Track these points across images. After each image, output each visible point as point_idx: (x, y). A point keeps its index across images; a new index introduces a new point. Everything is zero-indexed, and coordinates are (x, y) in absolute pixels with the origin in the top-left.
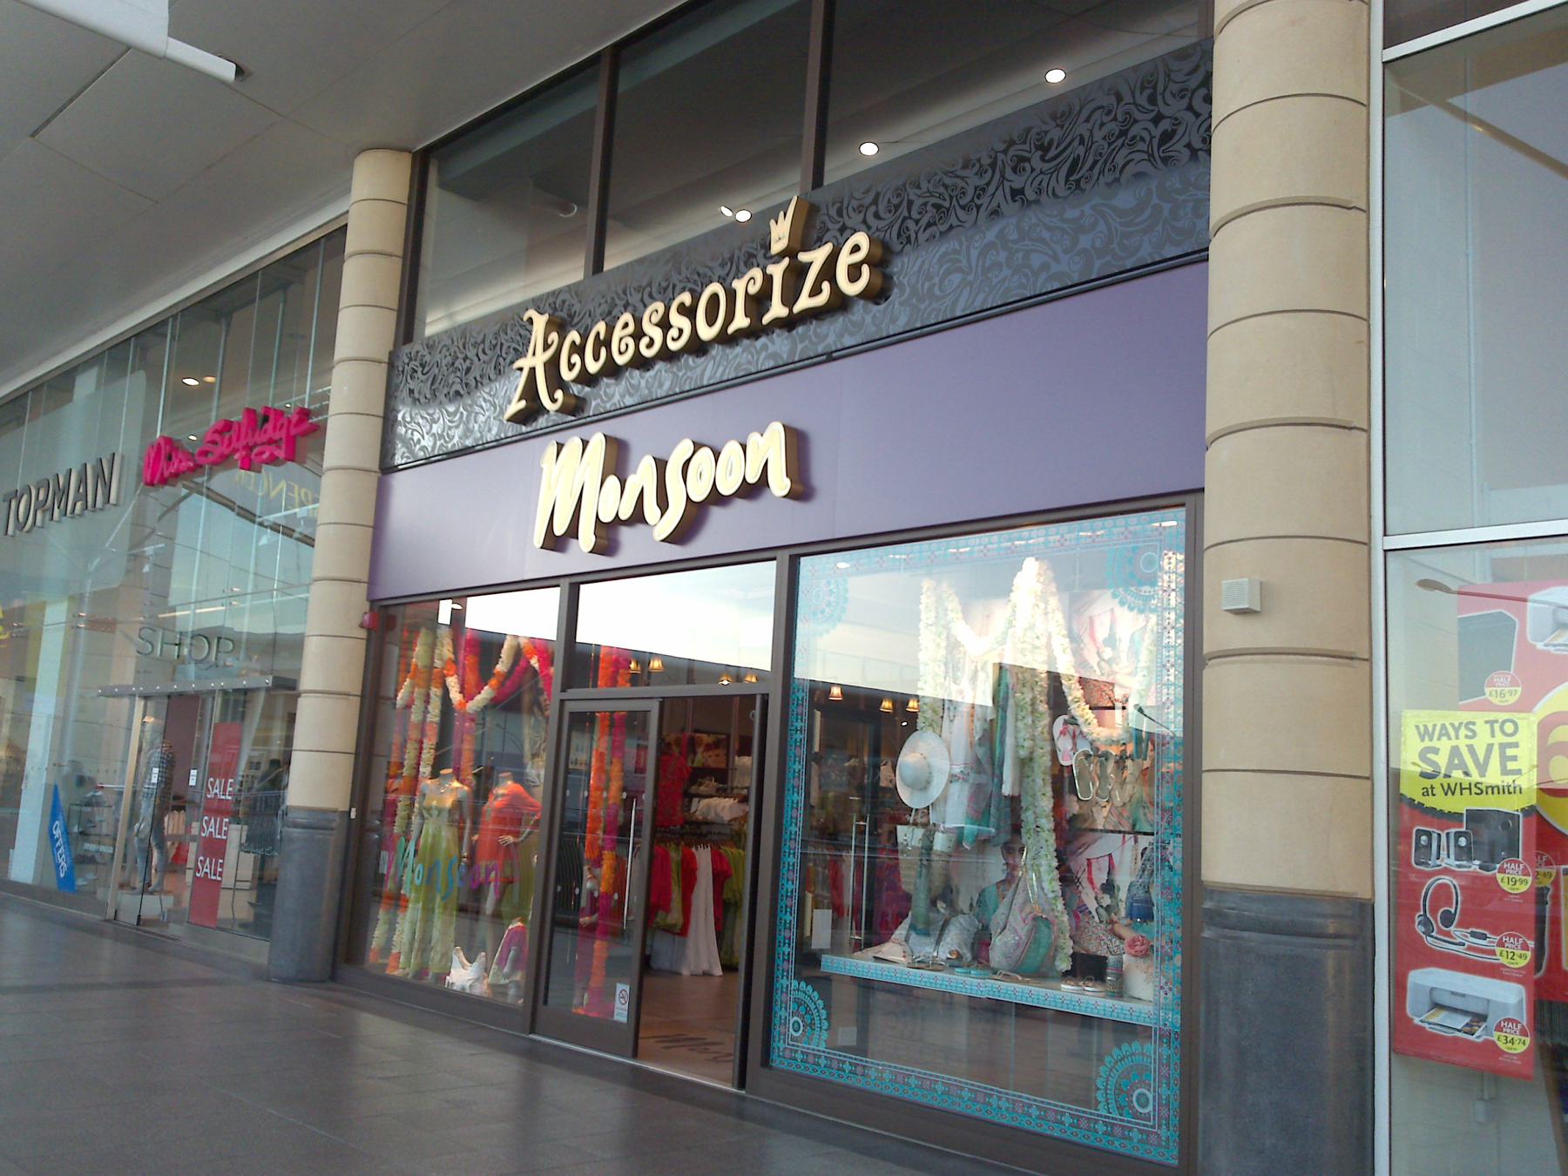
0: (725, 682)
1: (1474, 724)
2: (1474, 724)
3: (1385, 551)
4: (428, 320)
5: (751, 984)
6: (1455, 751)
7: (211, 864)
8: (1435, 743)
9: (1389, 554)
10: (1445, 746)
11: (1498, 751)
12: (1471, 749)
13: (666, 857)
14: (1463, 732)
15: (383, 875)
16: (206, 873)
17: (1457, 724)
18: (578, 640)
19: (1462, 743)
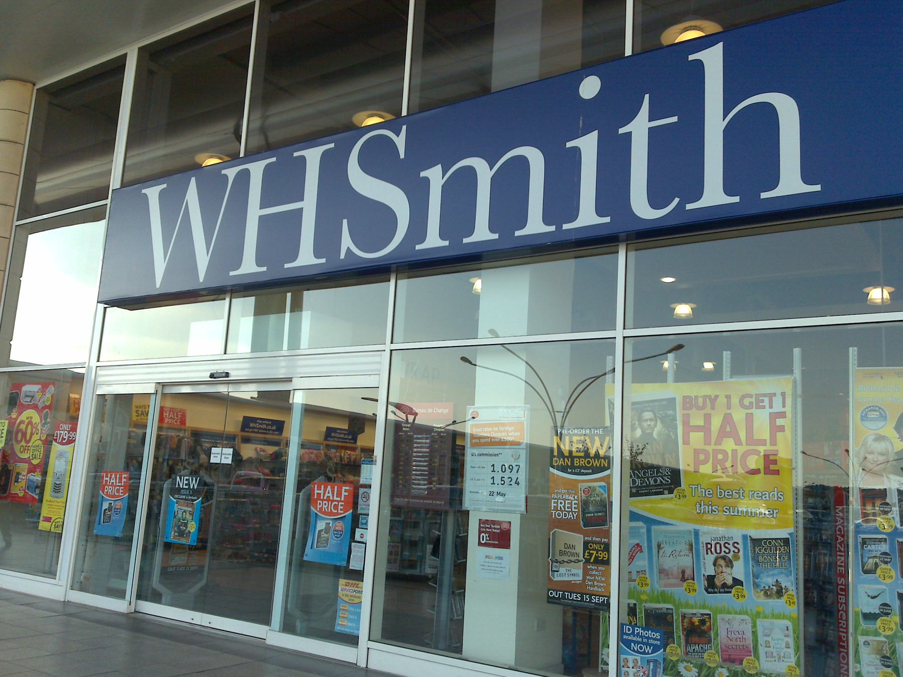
0: (437, 446)
1: (137, 416)
2: (137, 416)
3: (624, 337)
4: (38, 181)
5: (295, 510)
6: (142, 411)
7: (116, 478)
8: (138, 409)
9: (625, 338)
10: (140, 410)
11: (712, 436)
12: (145, 411)
13: (270, 421)
14: (140, 413)
15: (291, 404)
16: (113, 483)
17: (142, 416)
18: (10, 359)
19: (144, 410)
